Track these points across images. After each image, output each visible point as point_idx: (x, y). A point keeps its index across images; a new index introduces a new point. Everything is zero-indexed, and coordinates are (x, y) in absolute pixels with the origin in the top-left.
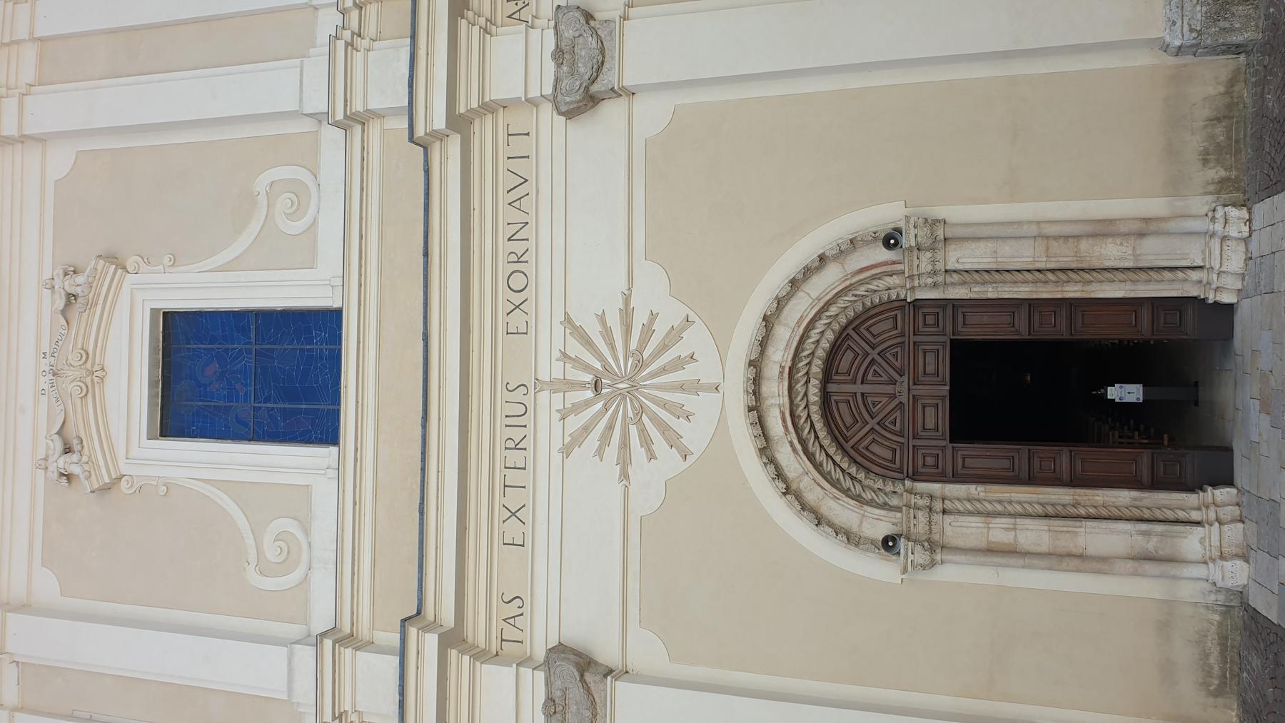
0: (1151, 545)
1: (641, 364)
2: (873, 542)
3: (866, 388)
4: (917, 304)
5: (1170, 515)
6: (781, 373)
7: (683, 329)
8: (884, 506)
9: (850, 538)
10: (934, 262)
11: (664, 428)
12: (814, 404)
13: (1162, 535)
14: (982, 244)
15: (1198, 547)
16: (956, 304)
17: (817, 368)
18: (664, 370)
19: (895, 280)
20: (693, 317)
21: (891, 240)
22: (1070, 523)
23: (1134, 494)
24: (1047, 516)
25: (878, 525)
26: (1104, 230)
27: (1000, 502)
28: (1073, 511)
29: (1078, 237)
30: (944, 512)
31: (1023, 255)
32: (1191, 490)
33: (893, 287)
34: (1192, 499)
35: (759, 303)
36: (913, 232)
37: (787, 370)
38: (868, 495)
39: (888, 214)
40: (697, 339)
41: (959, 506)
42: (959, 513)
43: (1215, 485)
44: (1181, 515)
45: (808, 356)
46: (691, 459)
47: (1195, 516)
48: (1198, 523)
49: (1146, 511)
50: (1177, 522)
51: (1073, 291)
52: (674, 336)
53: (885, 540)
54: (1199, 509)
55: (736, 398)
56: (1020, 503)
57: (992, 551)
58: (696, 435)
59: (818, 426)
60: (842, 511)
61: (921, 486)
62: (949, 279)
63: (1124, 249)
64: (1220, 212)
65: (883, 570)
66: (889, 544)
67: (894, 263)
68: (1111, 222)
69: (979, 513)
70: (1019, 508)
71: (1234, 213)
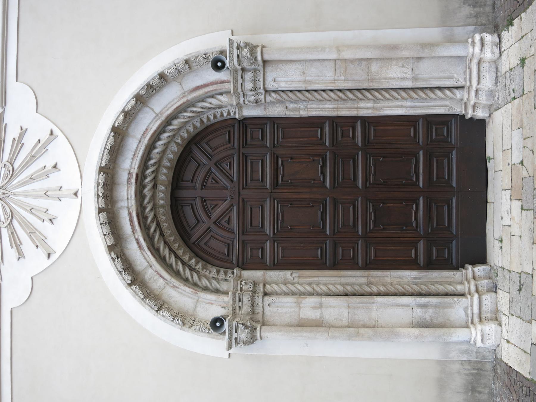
0: (428, 315)
1: (13, 174)
2: (202, 322)
3: (205, 194)
4: (245, 122)
5: (441, 288)
6: (129, 179)
7: (48, 142)
8: (217, 291)
9: (184, 319)
11: (32, 232)
12: (162, 206)
13: (436, 306)
14: (293, 66)
15: (462, 314)
16: (275, 122)
17: (165, 175)
19: (224, 99)
20: (56, 131)
22: (204, 230)
25: (212, 306)
27: (310, 284)
28: (367, 289)
29: (369, 60)
30: (265, 294)
31: (324, 77)
33: (227, 105)
34: (457, 275)
35: (111, 116)
36: (236, 52)
38: (205, 282)
39: (216, 41)
40: (60, 151)
41: (276, 288)
43: (473, 263)
45: (154, 165)
46: (54, 258)
47: (459, 288)
48: (463, 295)
49: (424, 287)
50: (447, 295)
51: (367, 108)
52: (41, 148)
54: (462, 283)
55: (91, 201)
56: (325, 284)
57: (303, 325)
58: (58, 237)
60: (180, 295)
62: (268, 99)
63: (405, 70)
65: (214, 346)
66: (217, 324)
67: (223, 82)
68: (394, 47)
69: (294, 294)
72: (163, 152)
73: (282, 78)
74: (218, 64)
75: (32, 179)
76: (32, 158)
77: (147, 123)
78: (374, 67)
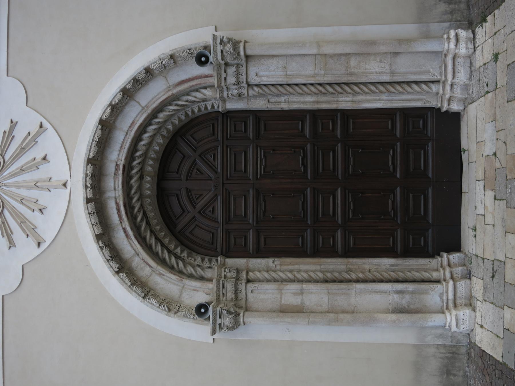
0: (405, 301)
4: (229, 115)
5: (417, 275)
6: (116, 170)
7: (38, 135)
8: (201, 278)
9: (170, 305)
10: (238, 75)
12: (149, 196)
13: (413, 292)
14: (275, 61)
15: (437, 299)
17: (151, 167)
18: (22, 170)
19: (208, 93)
20: (46, 124)
21: (202, 59)
23: (391, 261)
24: (326, 281)
25: (197, 293)
26: (367, 49)
27: (291, 271)
28: (346, 276)
29: (348, 55)
30: (248, 281)
31: (305, 72)
32: (432, 255)
33: (210, 98)
34: (433, 262)
35: (98, 110)
36: (219, 48)
37: (121, 168)
38: (190, 270)
39: (201, 36)
40: (50, 143)
42: (260, 281)
43: (449, 251)
44: (426, 275)
45: (140, 156)
46: (44, 246)
47: (435, 275)
48: (438, 281)
49: (401, 274)
50: (423, 281)
51: (346, 102)
52: (31, 141)
53: (200, 307)
54: (437, 270)
56: (306, 272)
57: (285, 310)
58: (48, 226)
59: (151, 215)
60: (166, 282)
61: (230, 261)
62: (251, 92)
63: (383, 65)
64: (452, 33)
65: (198, 332)
66: (201, 310)
67: (207, 76)
68: (372, 43)
69: (276, 281)
70: (305, 275)
71: (463, 34)
72: (150, 144)
73: (264, 73)
74: (202, 59)
75: (22, 170)
76: (22, 150)
77: (134, 115)
78: (353, 62)
